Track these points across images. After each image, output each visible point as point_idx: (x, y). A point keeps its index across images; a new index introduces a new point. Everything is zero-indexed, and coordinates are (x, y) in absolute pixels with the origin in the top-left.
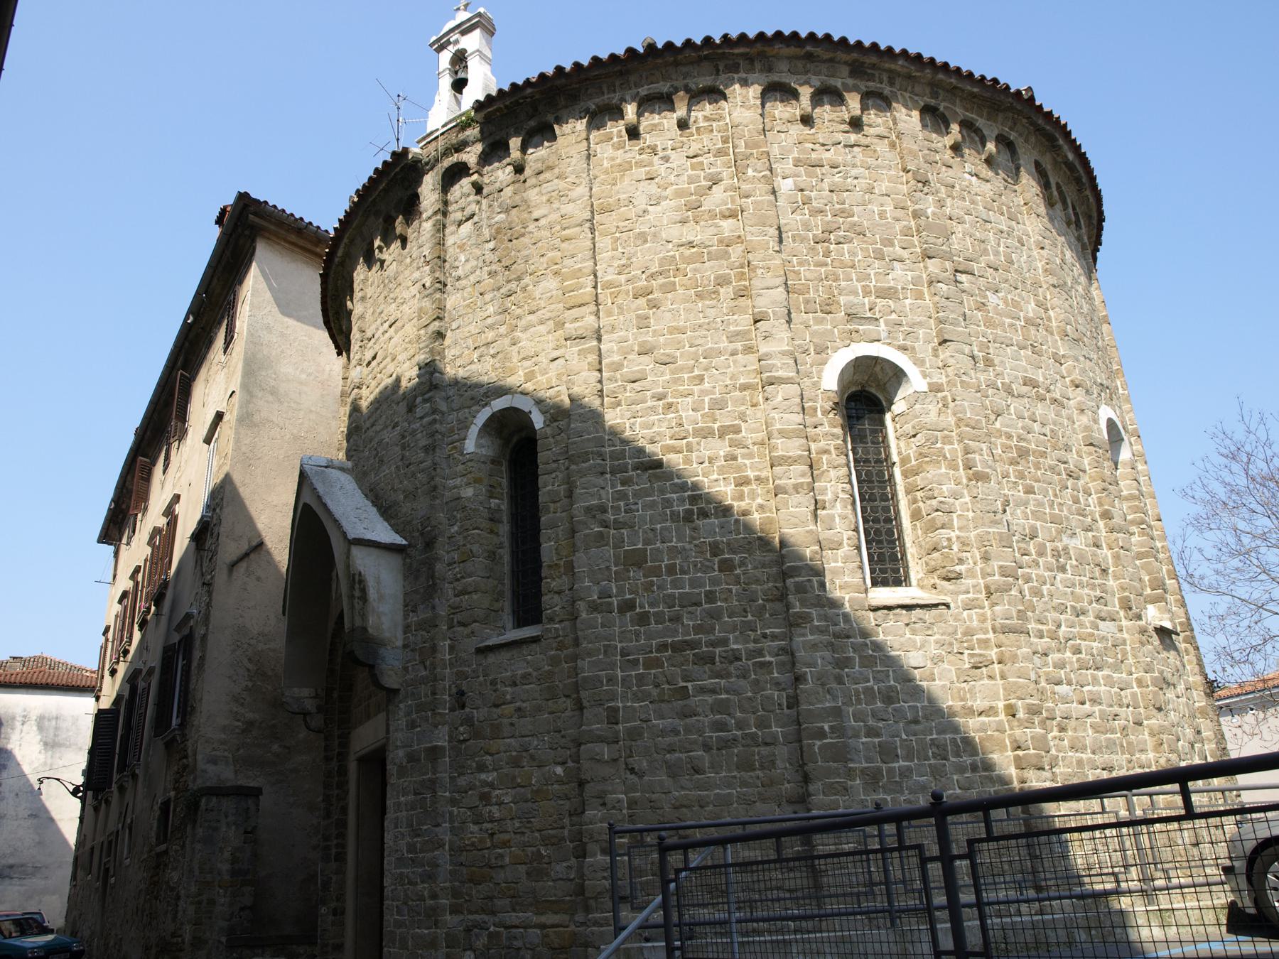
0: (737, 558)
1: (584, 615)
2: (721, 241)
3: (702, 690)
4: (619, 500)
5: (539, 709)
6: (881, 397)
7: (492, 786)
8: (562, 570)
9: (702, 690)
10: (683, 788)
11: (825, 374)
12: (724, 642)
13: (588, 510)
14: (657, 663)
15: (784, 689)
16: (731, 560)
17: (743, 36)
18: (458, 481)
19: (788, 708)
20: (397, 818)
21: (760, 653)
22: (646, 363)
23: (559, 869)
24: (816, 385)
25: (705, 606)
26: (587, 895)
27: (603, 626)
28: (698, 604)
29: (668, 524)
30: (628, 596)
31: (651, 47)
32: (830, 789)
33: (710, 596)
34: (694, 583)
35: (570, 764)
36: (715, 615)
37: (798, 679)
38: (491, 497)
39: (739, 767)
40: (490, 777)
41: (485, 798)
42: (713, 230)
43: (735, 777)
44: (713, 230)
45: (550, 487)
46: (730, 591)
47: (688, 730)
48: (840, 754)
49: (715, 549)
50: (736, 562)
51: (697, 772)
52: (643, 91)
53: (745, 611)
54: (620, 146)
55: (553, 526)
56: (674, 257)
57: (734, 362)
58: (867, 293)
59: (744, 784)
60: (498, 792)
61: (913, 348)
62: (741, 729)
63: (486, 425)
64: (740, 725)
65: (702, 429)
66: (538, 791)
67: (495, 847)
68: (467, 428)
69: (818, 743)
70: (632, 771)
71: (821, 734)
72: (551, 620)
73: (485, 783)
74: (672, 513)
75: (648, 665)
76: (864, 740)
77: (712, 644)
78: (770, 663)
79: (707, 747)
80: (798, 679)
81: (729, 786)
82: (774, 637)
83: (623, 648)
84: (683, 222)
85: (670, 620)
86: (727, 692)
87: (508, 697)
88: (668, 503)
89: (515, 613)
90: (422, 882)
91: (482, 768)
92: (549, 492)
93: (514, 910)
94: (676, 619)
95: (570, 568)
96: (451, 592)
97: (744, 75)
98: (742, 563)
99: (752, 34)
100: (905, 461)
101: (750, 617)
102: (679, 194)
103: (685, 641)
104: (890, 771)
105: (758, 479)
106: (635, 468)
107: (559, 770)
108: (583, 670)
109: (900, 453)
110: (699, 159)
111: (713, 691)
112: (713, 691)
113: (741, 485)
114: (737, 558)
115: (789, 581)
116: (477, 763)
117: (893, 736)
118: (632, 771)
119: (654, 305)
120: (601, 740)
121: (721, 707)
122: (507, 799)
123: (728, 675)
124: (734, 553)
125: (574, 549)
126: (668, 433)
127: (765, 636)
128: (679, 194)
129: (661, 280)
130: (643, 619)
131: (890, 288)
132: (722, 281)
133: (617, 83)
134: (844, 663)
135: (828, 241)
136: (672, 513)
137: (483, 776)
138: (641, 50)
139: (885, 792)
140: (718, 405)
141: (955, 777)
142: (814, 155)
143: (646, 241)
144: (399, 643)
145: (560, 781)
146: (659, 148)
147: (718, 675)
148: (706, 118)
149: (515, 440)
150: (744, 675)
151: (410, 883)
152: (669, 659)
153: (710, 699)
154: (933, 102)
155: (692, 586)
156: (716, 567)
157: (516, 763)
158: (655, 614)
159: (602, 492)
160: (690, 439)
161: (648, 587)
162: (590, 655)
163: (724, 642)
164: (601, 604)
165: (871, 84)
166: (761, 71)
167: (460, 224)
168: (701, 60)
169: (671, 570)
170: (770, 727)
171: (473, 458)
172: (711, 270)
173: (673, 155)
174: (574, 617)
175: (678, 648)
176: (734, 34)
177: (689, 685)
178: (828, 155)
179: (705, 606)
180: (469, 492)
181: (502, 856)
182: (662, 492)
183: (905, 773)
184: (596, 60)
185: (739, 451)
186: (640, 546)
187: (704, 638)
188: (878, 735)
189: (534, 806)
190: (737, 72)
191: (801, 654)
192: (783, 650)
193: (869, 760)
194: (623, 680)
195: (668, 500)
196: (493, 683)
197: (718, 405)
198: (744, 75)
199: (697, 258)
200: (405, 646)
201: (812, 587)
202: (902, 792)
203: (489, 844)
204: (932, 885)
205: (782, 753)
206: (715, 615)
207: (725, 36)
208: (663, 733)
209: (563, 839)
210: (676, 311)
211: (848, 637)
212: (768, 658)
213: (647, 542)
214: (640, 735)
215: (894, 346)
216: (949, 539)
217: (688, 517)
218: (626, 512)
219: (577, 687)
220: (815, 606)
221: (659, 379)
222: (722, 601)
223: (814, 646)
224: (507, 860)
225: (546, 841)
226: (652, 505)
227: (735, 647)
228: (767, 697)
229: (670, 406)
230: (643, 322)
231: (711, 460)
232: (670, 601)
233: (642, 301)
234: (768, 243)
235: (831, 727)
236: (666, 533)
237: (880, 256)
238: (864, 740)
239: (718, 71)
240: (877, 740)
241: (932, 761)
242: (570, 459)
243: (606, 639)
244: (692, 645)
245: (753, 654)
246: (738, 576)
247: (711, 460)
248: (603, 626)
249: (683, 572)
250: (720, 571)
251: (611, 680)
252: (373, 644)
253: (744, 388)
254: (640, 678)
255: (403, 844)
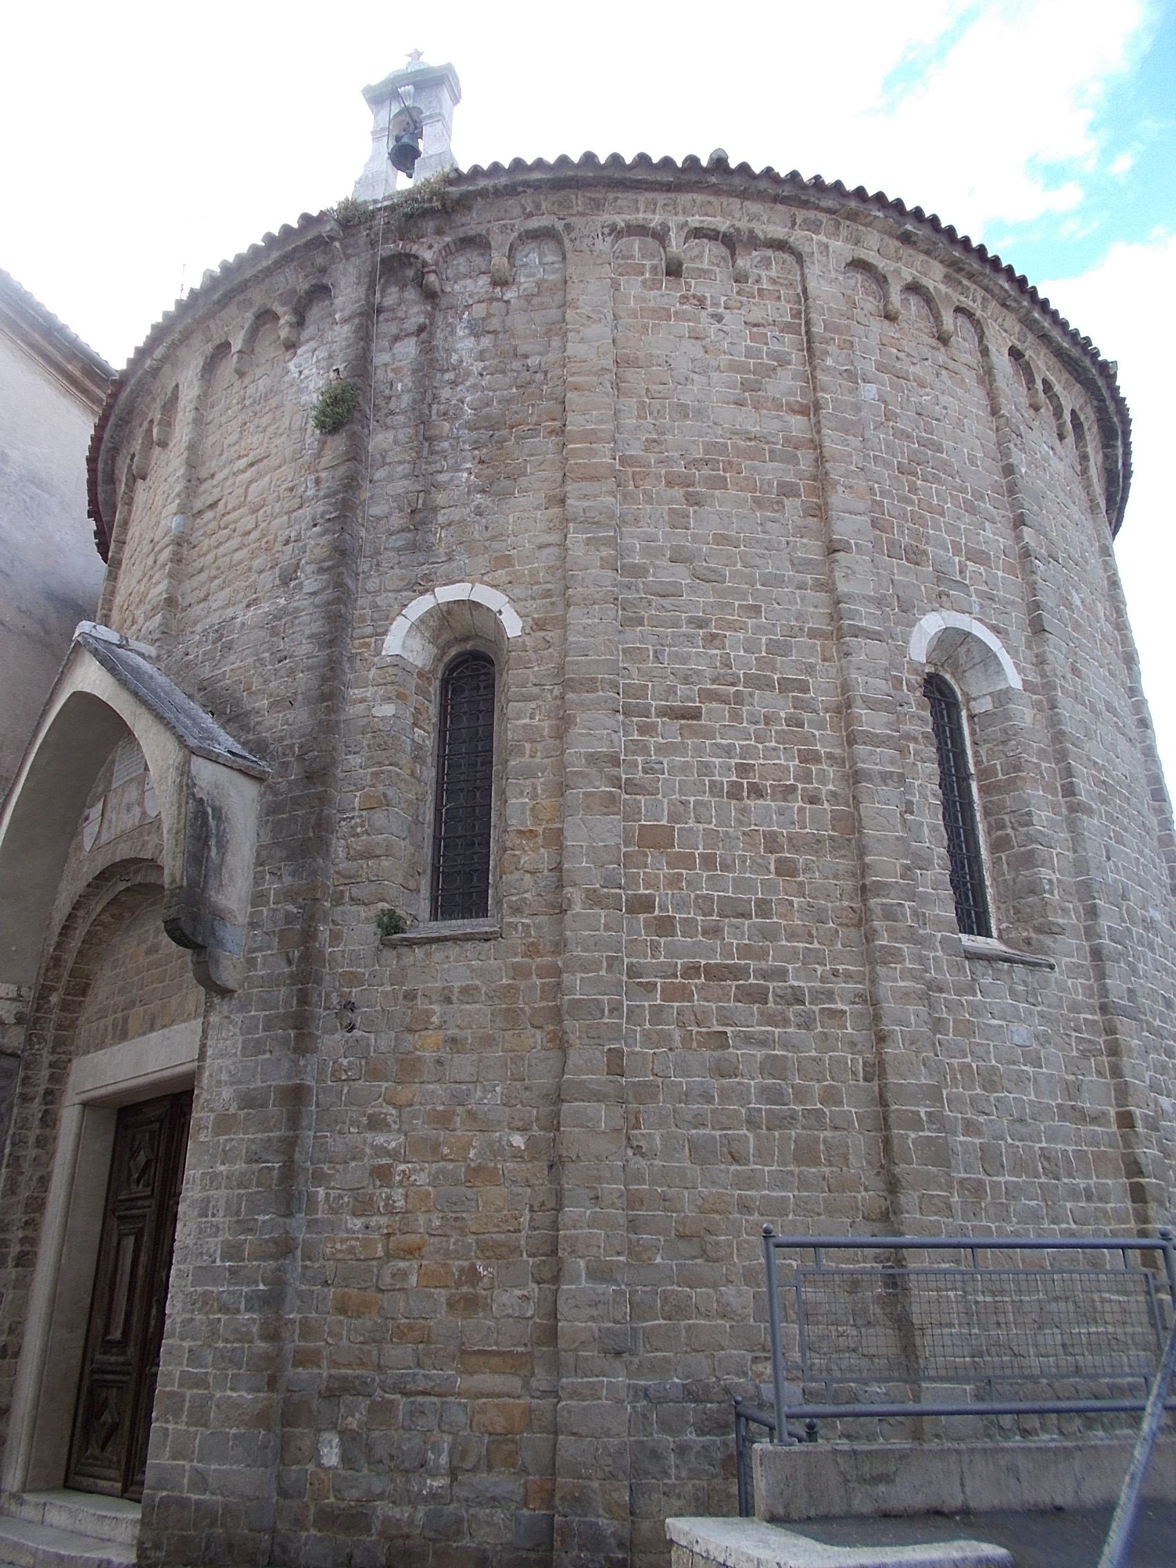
0: (801, 860)
1: (577, 909)
2: (787, 440)
3: (748, 1039)
4: (634, 753)
5: (488, 1041)
6: (956, 688)
7: (394, 1154)
8: (540, 840)
9: (748, 1039)
10: (714, 1183)
11: (913, 640)
12: (781, 974)
13: (592, 759)
14: (684, 994)
15: (860, 1052)
16: (793, 861)
17: (838, 185)
18: (369, 692)
19: (865, 1079)
20: (207, 1200)
21: (830, 995)
22: (681, 575)
23: (508, 1298)
24: (902, 651)
25: (755, 920)
26: (561, 1344)
27: (607, 928)
28: (745, 915)
29: (706, 798)
30: (642, 891)
31: (719, 162)
32: (926, 1203)
33: (763, 908)
34: (739, 884)
35: (536, 1131)
36: (769, 934)
37: (882, 1038)
38: (415, 724)
39: (798, 1160)
40: (392, 1141)
41: (382, 1174)
42: (777, 424)
43: (791, 1172)
44: (777, 424)
45: (527, 721)
46: (791, 903)
47: (725, 1096)
48: (941, 1155)
49: (772, 843)
50: (800, 866)
51: (735, 1159)
52: (695, 221)
53: (810, 935)
54: (654, 285)
55: (529, 773)
56: (725, 445)
57: (803, 598)
58: (957, 552)
59: (804, 1184)
60: (402, 1167)
61: (1007, 634)
62: (801, 1103)
63: (422, 620)
64: (801, 1095)
65: (758, 677)
66: (479, 1169)
67: (389, 1256)
68: (389, 619)
69: (913, 1135)
70: (638, 1150)
71: (916, 1123)
72: (517, 910)
73: (381, 1151)
74: (713, 784)
75: (671, 993)
76: (962, 1138)
77: (765, 975)
78: (843, 1012)
79: (752, 1123)
80: (882, 1038)
81: (783, 1186)
82: (848, 976)
83: (631, 966)
84: (740, 403)
85: (705, 933)
86: (784, 1046)
87: (434, 1019)
88: (705, 769)
89: (434, 899)
90: (247, 1310)
91: (376, 1124)
92: (525, 726)
93: (419, 1365)
94: (713, 932)
95: (556, 839)
96: (341, 853)
97: (825, 240)
98: (807, 869)
99: (850, 186)
100: (985, 773)
101: (816, 945)
102: (734, 367)
103: (726, 966)
104: (995, 1185)
105: (830, 756)
106: (662, 713)
107: (518, 1140)
108: (571, 991)
109: (977, 763)
110: (762, 330)
111: (763, 1043)
112: (763, 1043)
113: (807, 761)
114: (801, 860)
115: (873, 902)
116: (370, 1117)
117: (996, 1138)
118: (638, 1150)
119: (694, 500)
120: (598, 1097)
121: (773, 1067)
122: (421, 1179)
123: (786, 1022)
124: (797, 852)
125: (562, 812)
126: (708, 672)
127: (835, 973)
128: (734, 367)
129: (706, 471)
130: (664, 926)
131: (983, 552)
132: (788, 490)
133: (660, 203)
134: (938, 1025)
135: (914, 474)
136: (713, 784)
137: (380, 1139)
138: (704, 163)
139: (988, 1217)
140: (778, 649)
141: (1069, 1205)
142: (898, 365)
143: (686, 416)
144: (242, 919)
145: (517, 1155)
146: (708, 302)
147: (771, 1020)
148: (773, 281)
149: (453, 652)
150: (807, 1024)
151: (223, 1309)
152: (701, 988)
153: (759, 1054)
154: (1019, 346)
155: (736, 888)
156: (772, 868)
157: (443, 1120)
158: (684, 921)
159: (614, 736)
160: (741, 688)
161: (674, 882)
162: (584, 969)
163: (781, 974)
164: (607, 896)
165: (963, 298)
166: (847, 240)
167: (396, 338)
168: (776, 199)
169: (708, 861)
170: (841, 1103)
171: (398, 662)
172: (773, 472)
173: (728, 316)
174: (560, 910)
175: (714, 974)
176: (829, 180)
177: (729, 1030)
178: (912, 369)
179: (755, 920)
180: (388, 710)
181: (405, 1274)
182: (699, 750)
183: (1013, 1192)
184: (643, 159)
185: (806, 716)
186: (664, 822)
187: (753, 964)
188: (979, 1133)
189: (469, 1192)
190: (817, 232)
191: (889, 1005)
192: (860, 997)
193: (968, 1167)
194: (631, 1011)
195: (707, 765)
196: (410, 996)
197: (778, 649)
198: (825, 240)
199: (755, 454)
200: (253, 925)
201: (904, 915)
202: (1007, 1219)
203: (380, 1252)
204: (771, 1385)
205: (859, 1142)
206: (769, 934)
207: (817, 178)
208: (687, 1097)
209: (516, 1250)
210: (725, 510)
211: (941, 990)
212: (840, 1006)
213: (673, 817)
214: (654, 1097)
215: (986, 624)
216: (1050, 881)
217: (735, 792)
218: (645, 771)
219: (557, 1015)
220: (905, 940)
221: (701, 600)
222: (780, 916)
223: (906, 995)
224: (413, 1279)
225: (489, 1250)
226: (685, 768)
227: (796, 984)
228: (839, 1062)
229: (714, 637)
230: (678, 520)
231: (768, 720)
232: (704, 904)
233: (678, 492)
234: (851, 456)
235: (929, 1114)
236: (702, 810)
237: (971, 509)
238: (962, 1138)
239: (794, 223)
240: (977, 1141)
241: (1043, 1180)
242: (567, 685)
243: (611, 949)
244: (737, 973)
245: (817, 996)
246: (801, 884)
247: (768, 720)
248: (607, 928)
249: (725, 867)
250: (778, 873)
251: (615, 1009)
252: (219, 915)
253: (813, 634)
254: (657, 1012)
255: (214, 1244)
